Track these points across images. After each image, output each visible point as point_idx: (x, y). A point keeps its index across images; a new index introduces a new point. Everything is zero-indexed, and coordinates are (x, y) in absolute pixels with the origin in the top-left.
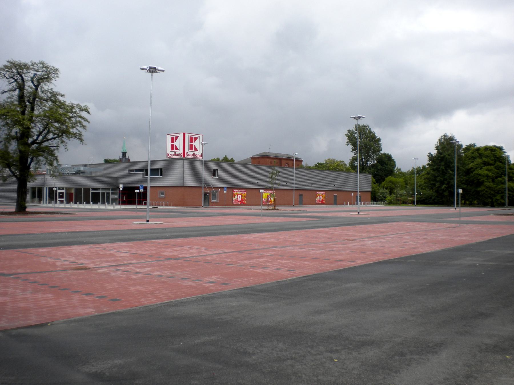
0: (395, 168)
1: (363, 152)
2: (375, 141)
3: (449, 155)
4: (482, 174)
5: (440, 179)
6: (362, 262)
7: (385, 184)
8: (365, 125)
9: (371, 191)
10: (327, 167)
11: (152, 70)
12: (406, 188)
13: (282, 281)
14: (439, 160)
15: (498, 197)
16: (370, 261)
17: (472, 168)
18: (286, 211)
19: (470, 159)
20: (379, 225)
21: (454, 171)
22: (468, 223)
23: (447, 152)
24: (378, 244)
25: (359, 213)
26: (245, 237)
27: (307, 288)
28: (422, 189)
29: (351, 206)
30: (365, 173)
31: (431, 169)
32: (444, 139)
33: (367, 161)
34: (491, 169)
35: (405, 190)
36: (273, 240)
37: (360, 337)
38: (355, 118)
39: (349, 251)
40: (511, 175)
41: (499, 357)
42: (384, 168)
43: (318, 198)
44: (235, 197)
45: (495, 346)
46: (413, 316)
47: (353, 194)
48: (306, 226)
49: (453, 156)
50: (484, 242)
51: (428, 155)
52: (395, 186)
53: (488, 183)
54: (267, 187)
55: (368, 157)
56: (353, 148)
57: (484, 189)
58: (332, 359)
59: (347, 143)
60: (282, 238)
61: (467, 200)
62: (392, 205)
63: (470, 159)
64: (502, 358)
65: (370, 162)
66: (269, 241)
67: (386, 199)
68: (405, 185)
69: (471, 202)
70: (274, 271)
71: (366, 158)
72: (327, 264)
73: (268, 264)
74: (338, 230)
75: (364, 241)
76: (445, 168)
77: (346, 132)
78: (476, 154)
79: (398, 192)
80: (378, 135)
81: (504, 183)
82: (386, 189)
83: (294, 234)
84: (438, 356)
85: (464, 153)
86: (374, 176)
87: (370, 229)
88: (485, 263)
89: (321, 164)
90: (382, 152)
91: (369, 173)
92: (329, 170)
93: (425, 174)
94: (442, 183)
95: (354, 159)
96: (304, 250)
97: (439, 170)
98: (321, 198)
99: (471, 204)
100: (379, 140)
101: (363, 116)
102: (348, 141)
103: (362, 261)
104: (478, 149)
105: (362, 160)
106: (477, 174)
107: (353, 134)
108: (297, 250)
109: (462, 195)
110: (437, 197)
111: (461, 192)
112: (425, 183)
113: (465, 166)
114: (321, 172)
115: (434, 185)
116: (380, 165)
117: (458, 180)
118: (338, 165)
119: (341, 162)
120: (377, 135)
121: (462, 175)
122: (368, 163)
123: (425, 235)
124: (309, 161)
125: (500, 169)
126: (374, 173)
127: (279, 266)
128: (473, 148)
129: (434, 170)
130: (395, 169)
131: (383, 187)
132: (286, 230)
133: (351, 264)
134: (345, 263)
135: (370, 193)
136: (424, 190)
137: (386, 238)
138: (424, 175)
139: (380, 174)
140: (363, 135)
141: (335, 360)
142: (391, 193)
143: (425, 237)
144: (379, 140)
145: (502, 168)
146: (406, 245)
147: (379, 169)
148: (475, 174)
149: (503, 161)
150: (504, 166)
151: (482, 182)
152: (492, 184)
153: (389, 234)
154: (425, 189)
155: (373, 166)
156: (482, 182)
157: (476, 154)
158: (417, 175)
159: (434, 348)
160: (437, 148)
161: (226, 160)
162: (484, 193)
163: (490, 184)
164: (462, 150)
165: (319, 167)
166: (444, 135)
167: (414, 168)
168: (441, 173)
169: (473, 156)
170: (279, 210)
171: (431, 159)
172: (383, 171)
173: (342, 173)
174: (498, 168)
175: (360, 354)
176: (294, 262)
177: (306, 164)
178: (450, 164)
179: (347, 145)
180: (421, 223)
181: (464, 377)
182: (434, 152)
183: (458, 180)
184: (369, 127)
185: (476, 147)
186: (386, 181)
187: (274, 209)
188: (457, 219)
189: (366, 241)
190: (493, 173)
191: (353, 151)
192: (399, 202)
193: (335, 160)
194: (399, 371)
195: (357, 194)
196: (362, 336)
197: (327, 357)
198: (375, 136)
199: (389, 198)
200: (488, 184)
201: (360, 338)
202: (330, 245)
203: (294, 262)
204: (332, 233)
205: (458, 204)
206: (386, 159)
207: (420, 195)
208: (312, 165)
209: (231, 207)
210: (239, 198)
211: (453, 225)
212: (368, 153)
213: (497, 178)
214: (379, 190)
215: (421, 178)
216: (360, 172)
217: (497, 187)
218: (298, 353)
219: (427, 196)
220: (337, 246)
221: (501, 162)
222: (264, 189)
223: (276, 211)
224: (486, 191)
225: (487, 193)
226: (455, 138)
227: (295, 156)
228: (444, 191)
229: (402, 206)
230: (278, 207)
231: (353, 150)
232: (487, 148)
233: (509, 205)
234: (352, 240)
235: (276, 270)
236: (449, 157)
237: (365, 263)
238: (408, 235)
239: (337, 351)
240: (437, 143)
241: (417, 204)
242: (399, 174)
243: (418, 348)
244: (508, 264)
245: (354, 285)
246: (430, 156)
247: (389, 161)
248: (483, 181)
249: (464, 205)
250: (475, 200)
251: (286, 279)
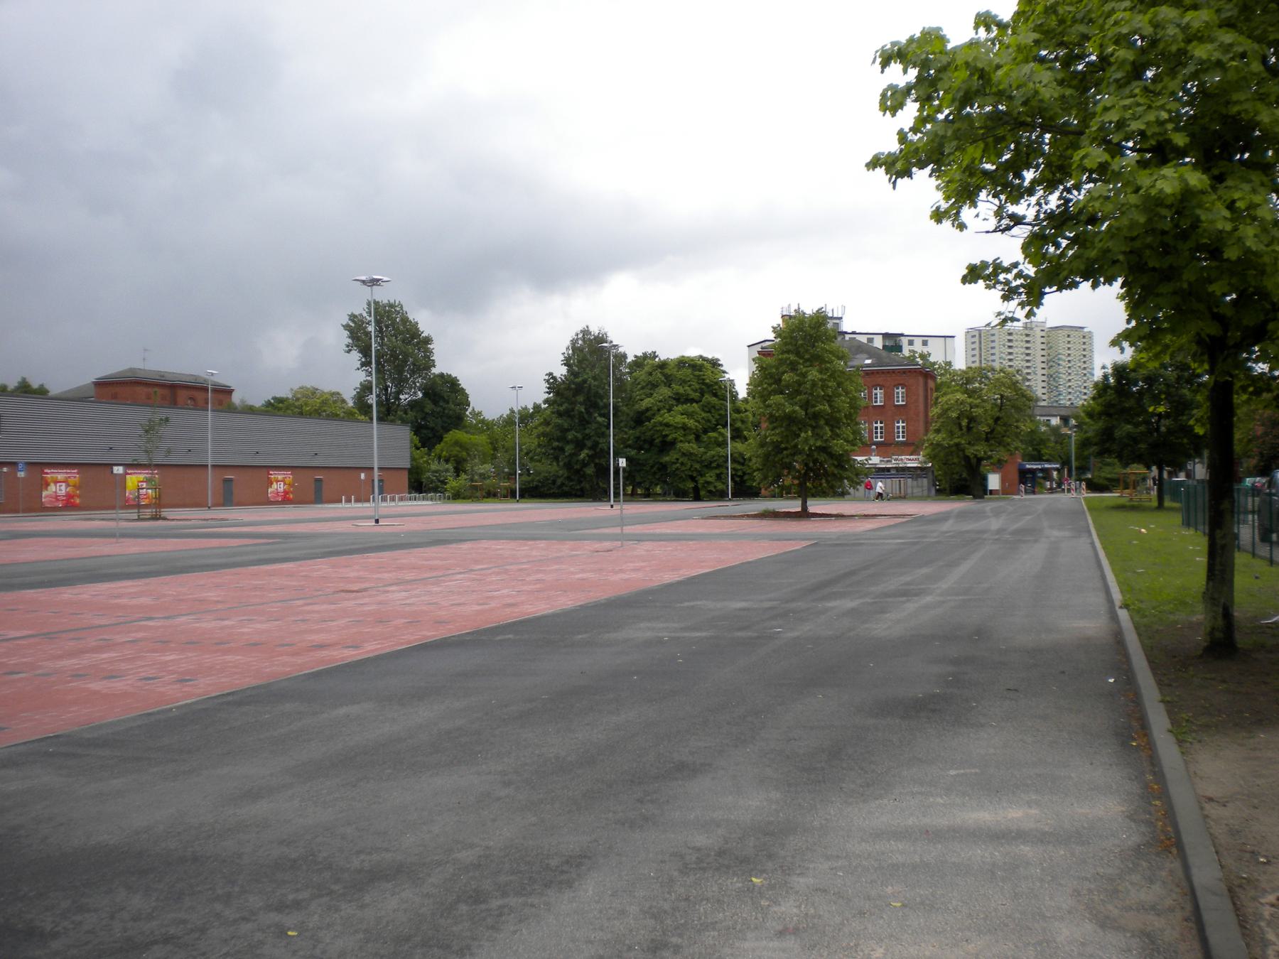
0: (467, 410)
1: (388, 370)
2: (418, 343)
3: (595, 378)
4: (672, 422)
5: (576, 437)
6: (379, 646)
7: (442, 451)
8: (392, 301)
9: (409, 466)
10: (296, 407)
11: (144, 359)
12: (496, 458)
13: (158, 713)
14: (571, 389)
15: (710, 476)
16: (402, 644)
17: (648, 410)
18: (188, 523)
19: (643, 388)
20: (427, 549)
21: (607, 416)
22: (640, 538)
23: (591, 371)
24: (423, 598)
25: (377, 521)
26: (67, 593)
27: (226, 728)
28: (532, 459)
29: (359, 505)
30: (393, 422)
31: (553, 413)
32: (583, 339)
33: (399, 392)
34: (693, 412)
35: (492, 464)
36: (144, 600)
37: (362, 857)
38: (363, 282)
39: (348, 620)
40: (739, 424)
41: (735, 883)
42: (439, 409)
43: (275, 486)
44: (49, 488)
45: (721, 853)
46: (507, 784)
47: (363, 476)
48: (238, 559)
49: (604, 381)
50: (679, 583)
51: (547, 378)
52: (468, 454)
53: (687, 444)
54: (135, 460)
55: (401, 383)
56: (363, 360)
57: (677, 459)
58: (281, 932)
59: (348, 346)
60: (170, 593)
61: (639, 484)
62: (460, 500)
63: (643, 388)
64: (740, 885)
65: (407, 396)
66: (135, 602)
67: (447, 486)
68: (492, 452)
69: (648, 489)
70: (139, 684)
71: (396, 386)
72: (285, 658)
73: (124, 666)
74: (322, 567)
75: (388, 592)
76: (585, 409)
77: (345, 320)
78: (658, 375)
79: (476, 468)
80: (425, 328)
81: (723, 444)
82: (447, 461)
83: (202, 583)
84: (572, 895)
85: (630, 373)
86: (417, 430)
87: (404, 561)
88: (686, 634)
89: (281, 400)
90: (435, 371)
91: (404, 422)
92: (301, 414)
93: (541, 424)
94: (580, 445)
95: (366, 388)
96: (226, 623)
97: (572, 413)
98: (282, 486)
99: (648, 496)
100: (428, 340)
101: (385, 279)
102: (350, 341)
103: (379, 644)
104: (663, 365)
105: (386, 390)
106: (661, 424)
107: (360, 326)
108: (208, 624)
109: (626, 474)
110: (569, 478)
111: (624, 465)
112: (539, 445)
113: (633, 405)
114: (280, 419)
115: (562, 450)
116: (429, 402)
117: (617, 438)
118: (324, 402)
119: (333, 394)
120: (421, 327)
121: (626, 426)
122: (401, 397)
123: (538, 572)
124: (250, 392)
125: (713, 411)
126: (417, 421)
127: (154, 671)
128: (651, 362)
129: (560, 414)
130: (467, 413)
131: (439, 458)
132: (181, 572)
133: (350, 655)
134: (335, 653)
135: (406, 473)
136: (538, 464)
137: (445, 581)
138: (536, 428)
139: (431, 425)
140: (387, 327)
141: (290, 933)
142: (458, 471)
143: (540, 576)
144: (428, 340)
145: (718, 410)
146: (492, 598)
147: (427, 414)
148: (655, 423)
149: (719, 394)
150: (722, 404)
151: (673, 443)
152: (695, 446)
153: (451, 572)
154: (540, 461)
155: (413, 405)
156: (673, 443)
157: (658, 375)
158: (519, 426)
159: (562, 872)
160: (567, 362)
161: (24, 389)
162: (677, 469)
163: (692, 447)
164: (626, 368)
165: (277, 407)
166: (581, 331)
167: (512, 411)
168: (577, 421)
169: (650, 382)
170: (168, 520)
171: (554, 388)
172: (437, 418)
173: (336, 422)
174: (709, 408)
175: (362, 907)
176: (196, 656)
177: (242, 401)
178: (599, 401)
179: (349, 351)
180: (530, 543)
181: (645, 949)
182: (561, 371)
183: (617, 438)
184: (402, 308)
185: (657, 360)
186: (446, 443)
187: (156, 518)
188: (617, 530)
189: (393, 591)
190: (696, 421)
191: (362, 367)
192: (478, 494)
193: (317, 389)
194: (468, 947)
195: (373, 476)
196: (370, 853)
197: (269, 927)
198: (418, 330)
199: (453, 483)
200: (685, 446)
201: (363, 861)
202: (299, 606)
203: (196, 656)
204: (305, 576)
205: (617, 495)
206: (446, 389)
207: (529, 474)
208: (258, 402)
209: (38, 514)
210: (60, 490)
211: (607, 545)
212: (400, 372)
213: (705, 431)
214: (429, 464)
215: (531, 435)
216: (380, 419)
217: (706, 453)
218: (184, 922)
219: (545, 477)
220: (316, 608)
221: (715, 395)
222: (127, 466)
223: (160, 523)
224: (682, 464)
225: (683, 468)
226: (609, 339)
227: (212, 378)
228: (585, 465)
229: (486, 502)
230: (166, 512)
231: (363, 365)
232: (683, 363)
233: (734, 495)
234: (357, 591)
235: (144, 682)
236: (596, 383)
237: (388, 650)
238: (498, 573)
239: (297, 905)
240: (568, 348)
241: (522, 496)
242: (477, 424)
243: (521, 876)
244: (740, 634)
245: (354, 709)
246: (551, 381)
247: (452, 392)
248: (675, 439)
249: (632, 497)
250: (657, 484)
251: (168, 706)
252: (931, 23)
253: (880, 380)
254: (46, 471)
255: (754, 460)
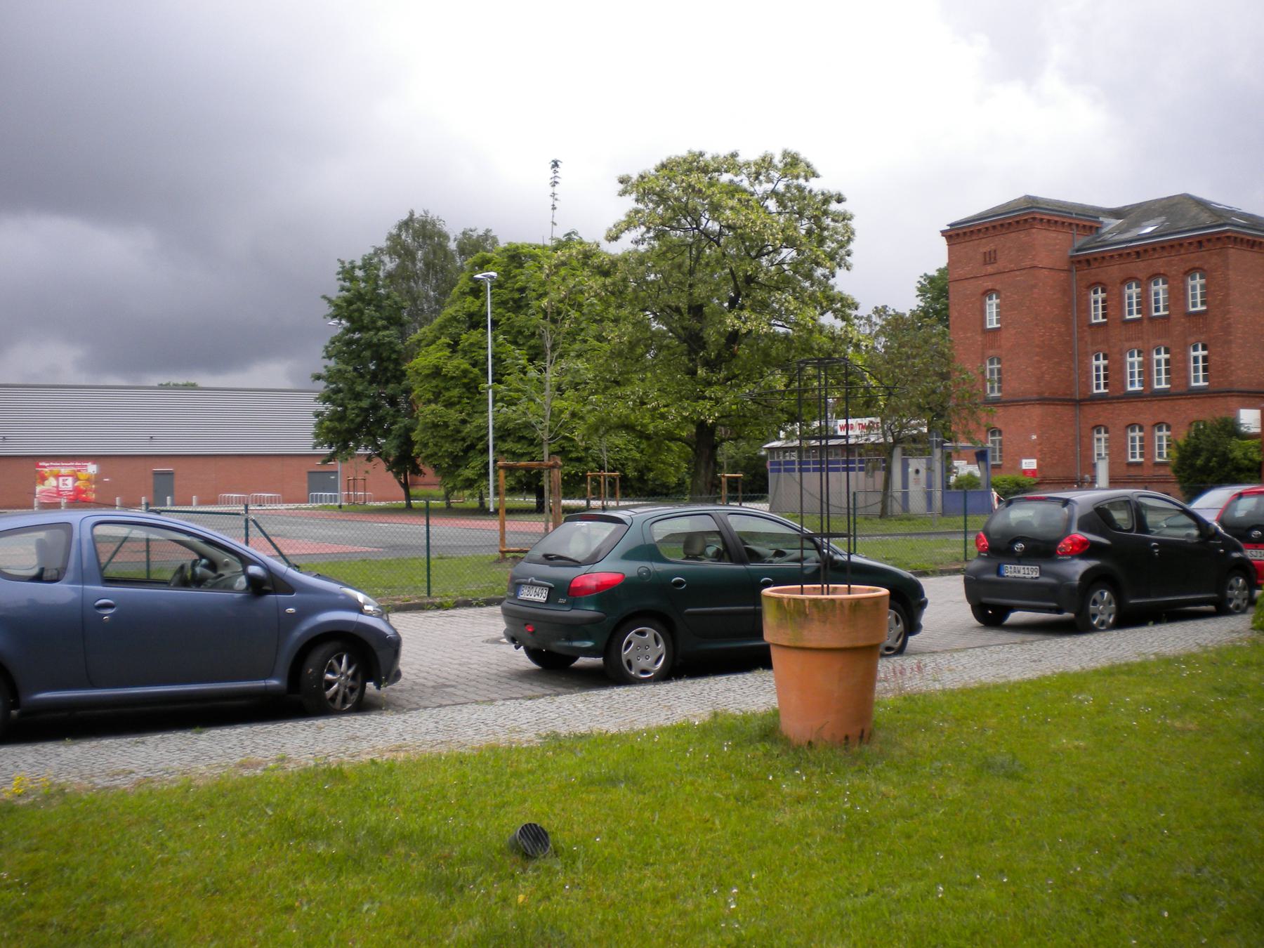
44: (46, 482)
252: (848, 199)
253: (1159, 264)
254: (41, 464)
255: (292, 765)
